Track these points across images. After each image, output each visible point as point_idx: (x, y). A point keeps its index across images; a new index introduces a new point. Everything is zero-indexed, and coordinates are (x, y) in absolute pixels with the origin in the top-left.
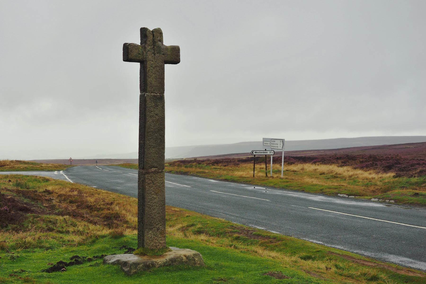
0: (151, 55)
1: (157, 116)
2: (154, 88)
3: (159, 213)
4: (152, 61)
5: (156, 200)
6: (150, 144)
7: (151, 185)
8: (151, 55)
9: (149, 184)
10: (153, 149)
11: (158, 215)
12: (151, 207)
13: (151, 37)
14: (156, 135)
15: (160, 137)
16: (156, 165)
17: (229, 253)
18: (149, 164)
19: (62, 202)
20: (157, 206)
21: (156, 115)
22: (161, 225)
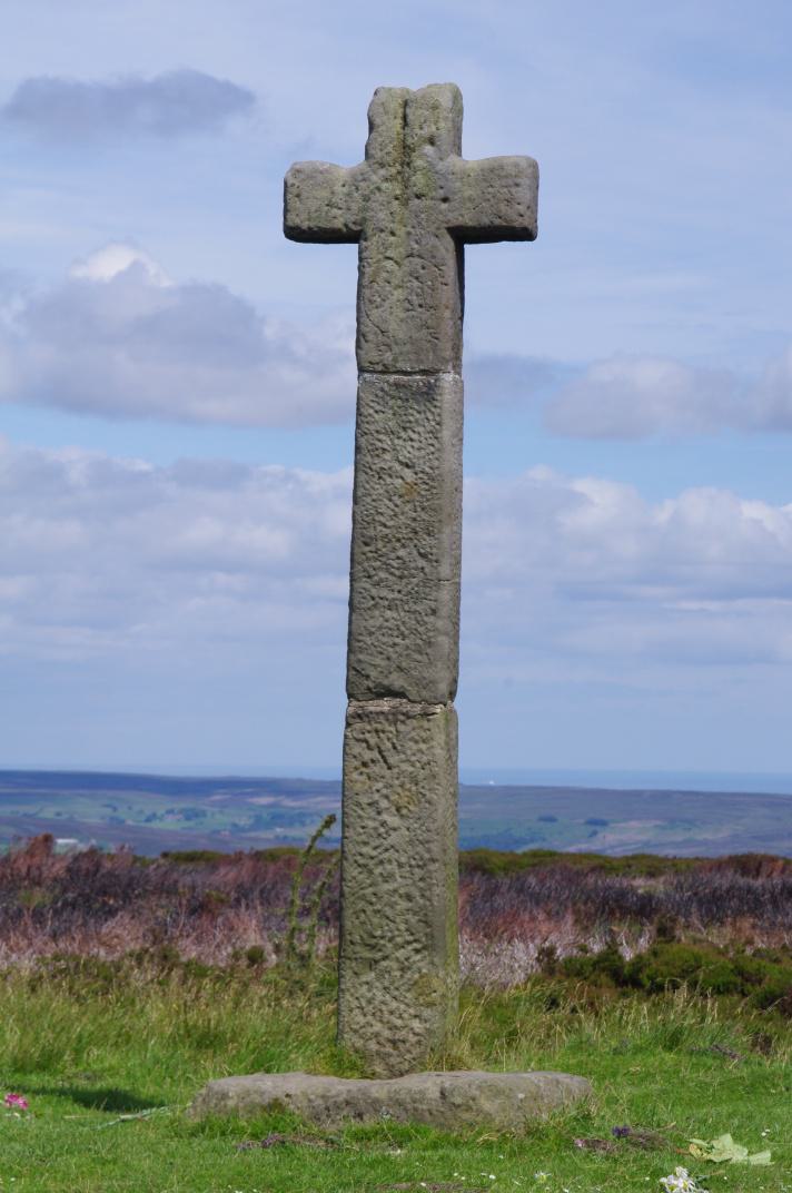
0: (418, 221)
1: (408, 473)
2: (396, 349)
3: (409, 898)
4: (393, 234)
5: (394, 838)
6: (374, 592)
7: (376, 769)
8: (418, 221)
9: (365, 764)
10: (389, 614)
11: (403, 904)
12: (371, 863)
13: (409, 132)
14: (401, 553)
15: (421, 563)
16: (397, 681)
17: (645, 1008)
18: (368, 677)
19: (138, 978)
20: (400, 865)
21: (407, 466)
22: (417, 951)
